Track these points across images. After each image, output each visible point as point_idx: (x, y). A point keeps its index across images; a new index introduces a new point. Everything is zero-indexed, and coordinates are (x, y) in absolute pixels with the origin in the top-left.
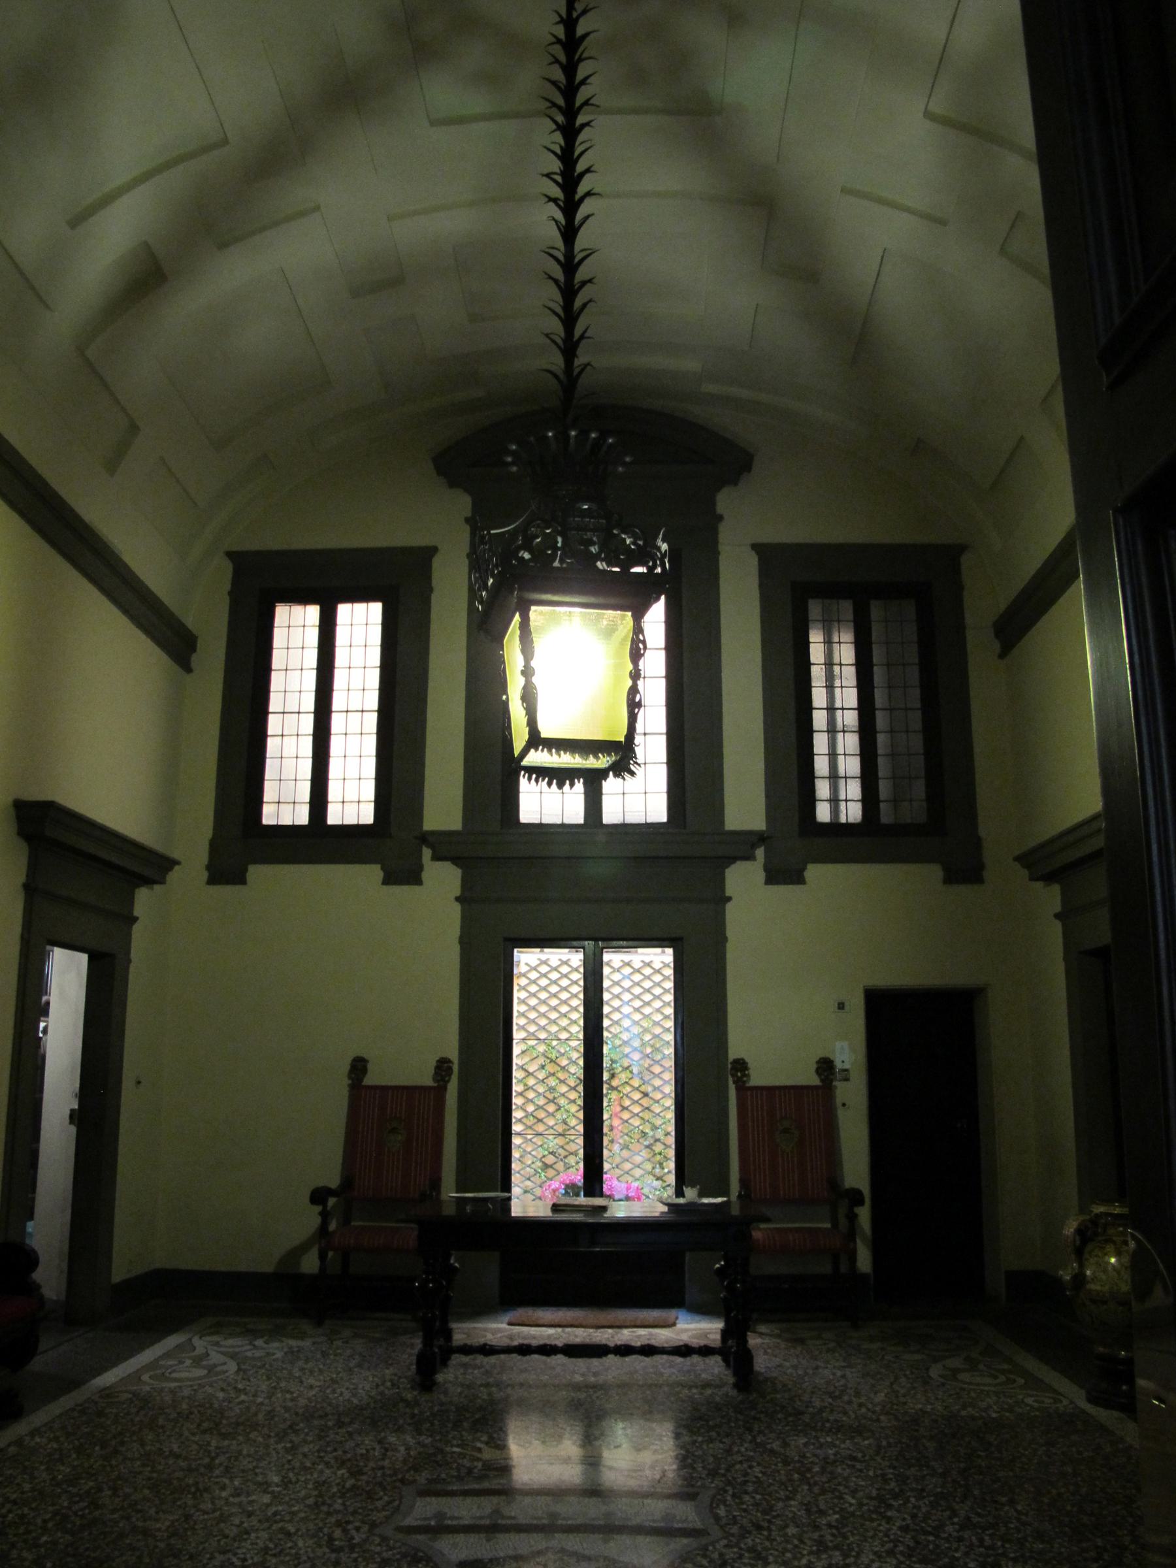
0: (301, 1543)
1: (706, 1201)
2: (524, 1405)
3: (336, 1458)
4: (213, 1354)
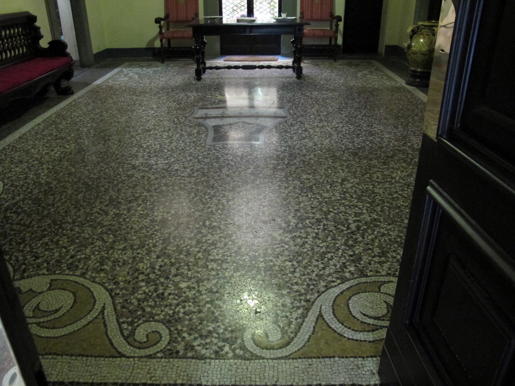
0: (165, 123)
1: (289, 18)
2: (230, 85)
3: (173, 100)
4: (130, 73)
